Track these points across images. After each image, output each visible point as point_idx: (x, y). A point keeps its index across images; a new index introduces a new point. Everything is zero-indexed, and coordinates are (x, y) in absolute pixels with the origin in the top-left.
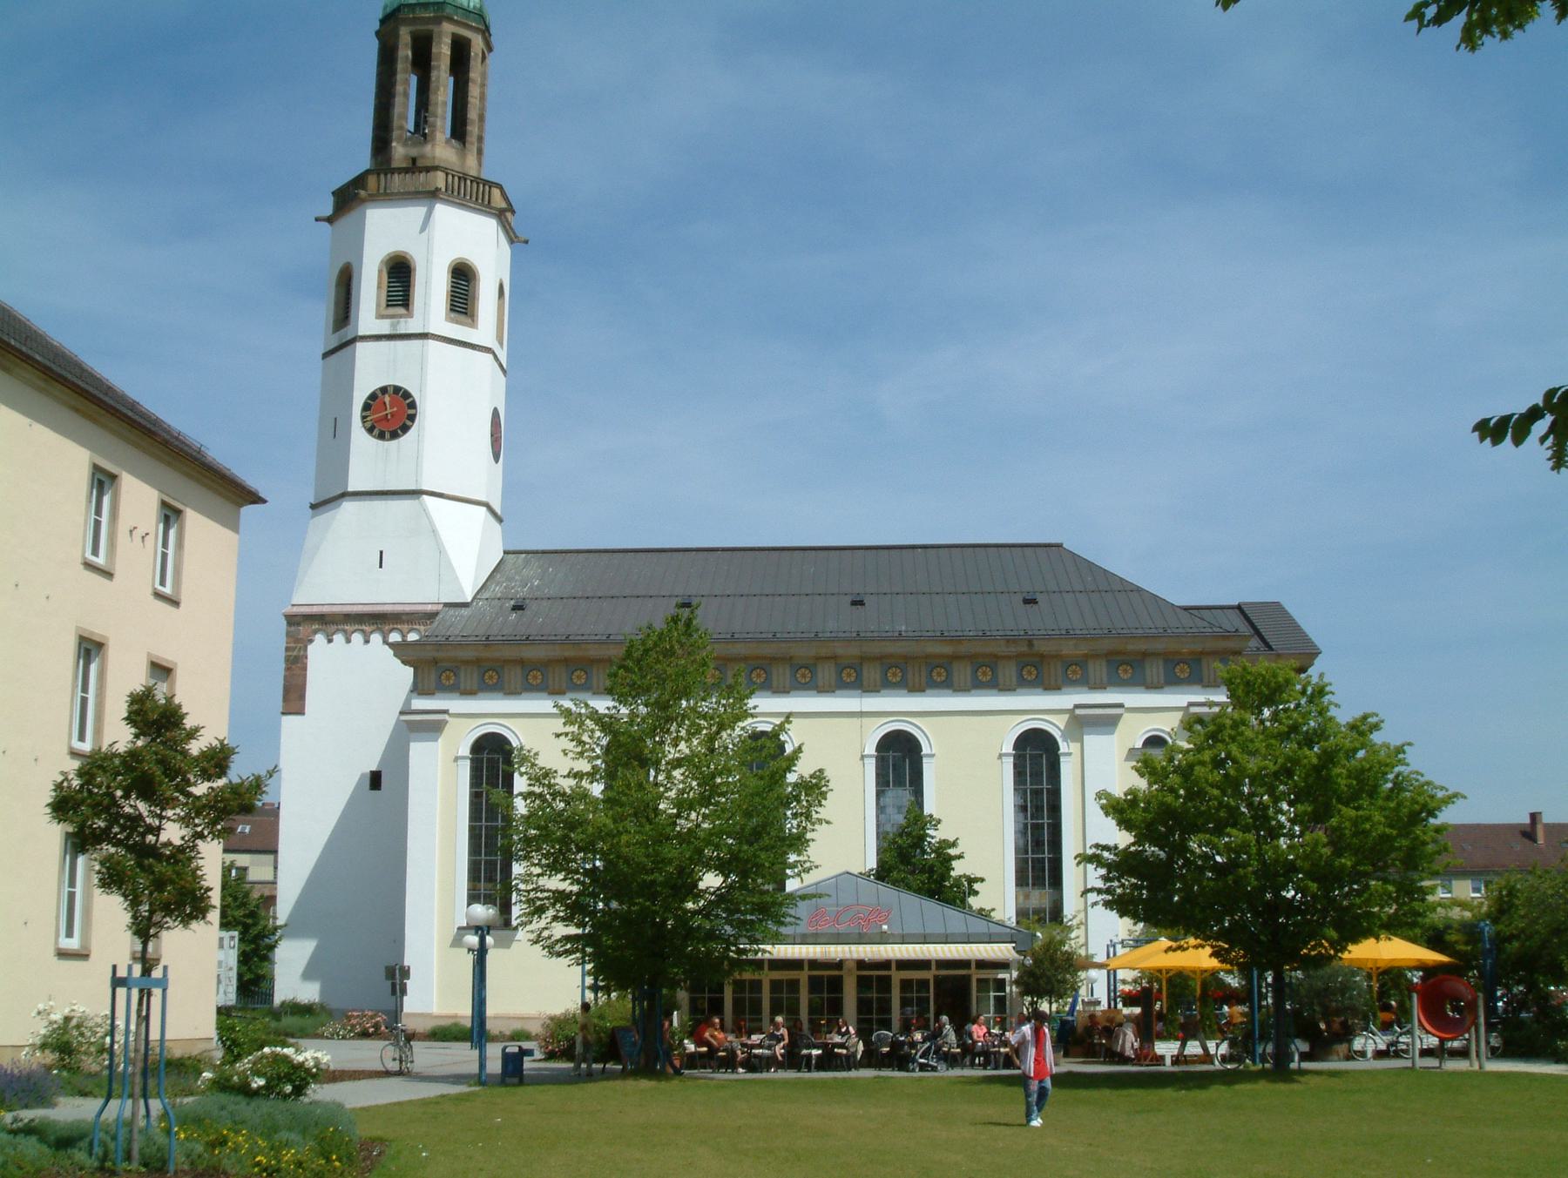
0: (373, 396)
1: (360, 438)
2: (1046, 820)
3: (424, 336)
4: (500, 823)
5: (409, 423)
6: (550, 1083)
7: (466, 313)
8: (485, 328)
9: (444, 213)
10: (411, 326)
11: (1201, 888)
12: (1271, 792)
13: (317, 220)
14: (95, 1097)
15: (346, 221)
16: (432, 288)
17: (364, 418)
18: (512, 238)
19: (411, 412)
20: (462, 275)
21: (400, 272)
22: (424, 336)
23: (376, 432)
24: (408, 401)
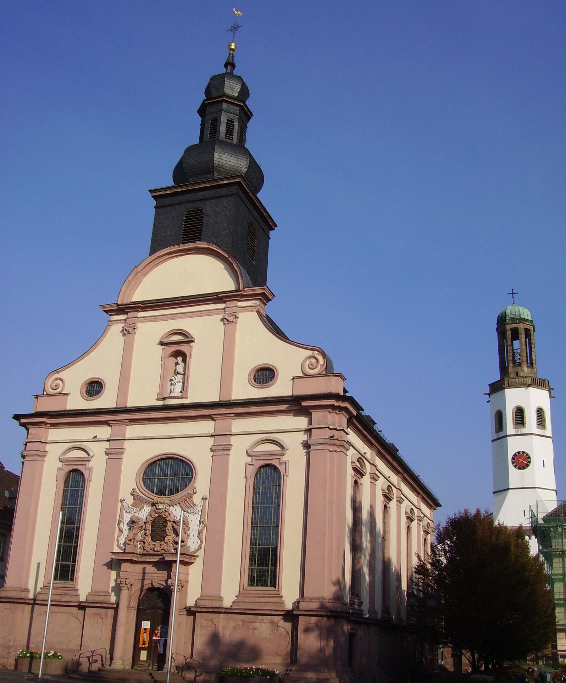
0: (515, 455)
1: (512, 469)
2: (270, 568)
3: (532, 434)
4: (78, 506)
5: (529, 464)
6: (29, 668)
7: (542, 425)
8: (548, 431)
9: (532, 390)
10: (524, 431)
11: (253, 671)
12: (434, 585)
13: (484, 394)
14: (287, 665)
15: (495, 396)
16: (531, 418)
17: (513, 463)
18: (551, 397)
19: (529, 460)
20: (540, 412)
21: (520, 413)
22: (532, 434)
23: (517, 467)
24: (528, 456)
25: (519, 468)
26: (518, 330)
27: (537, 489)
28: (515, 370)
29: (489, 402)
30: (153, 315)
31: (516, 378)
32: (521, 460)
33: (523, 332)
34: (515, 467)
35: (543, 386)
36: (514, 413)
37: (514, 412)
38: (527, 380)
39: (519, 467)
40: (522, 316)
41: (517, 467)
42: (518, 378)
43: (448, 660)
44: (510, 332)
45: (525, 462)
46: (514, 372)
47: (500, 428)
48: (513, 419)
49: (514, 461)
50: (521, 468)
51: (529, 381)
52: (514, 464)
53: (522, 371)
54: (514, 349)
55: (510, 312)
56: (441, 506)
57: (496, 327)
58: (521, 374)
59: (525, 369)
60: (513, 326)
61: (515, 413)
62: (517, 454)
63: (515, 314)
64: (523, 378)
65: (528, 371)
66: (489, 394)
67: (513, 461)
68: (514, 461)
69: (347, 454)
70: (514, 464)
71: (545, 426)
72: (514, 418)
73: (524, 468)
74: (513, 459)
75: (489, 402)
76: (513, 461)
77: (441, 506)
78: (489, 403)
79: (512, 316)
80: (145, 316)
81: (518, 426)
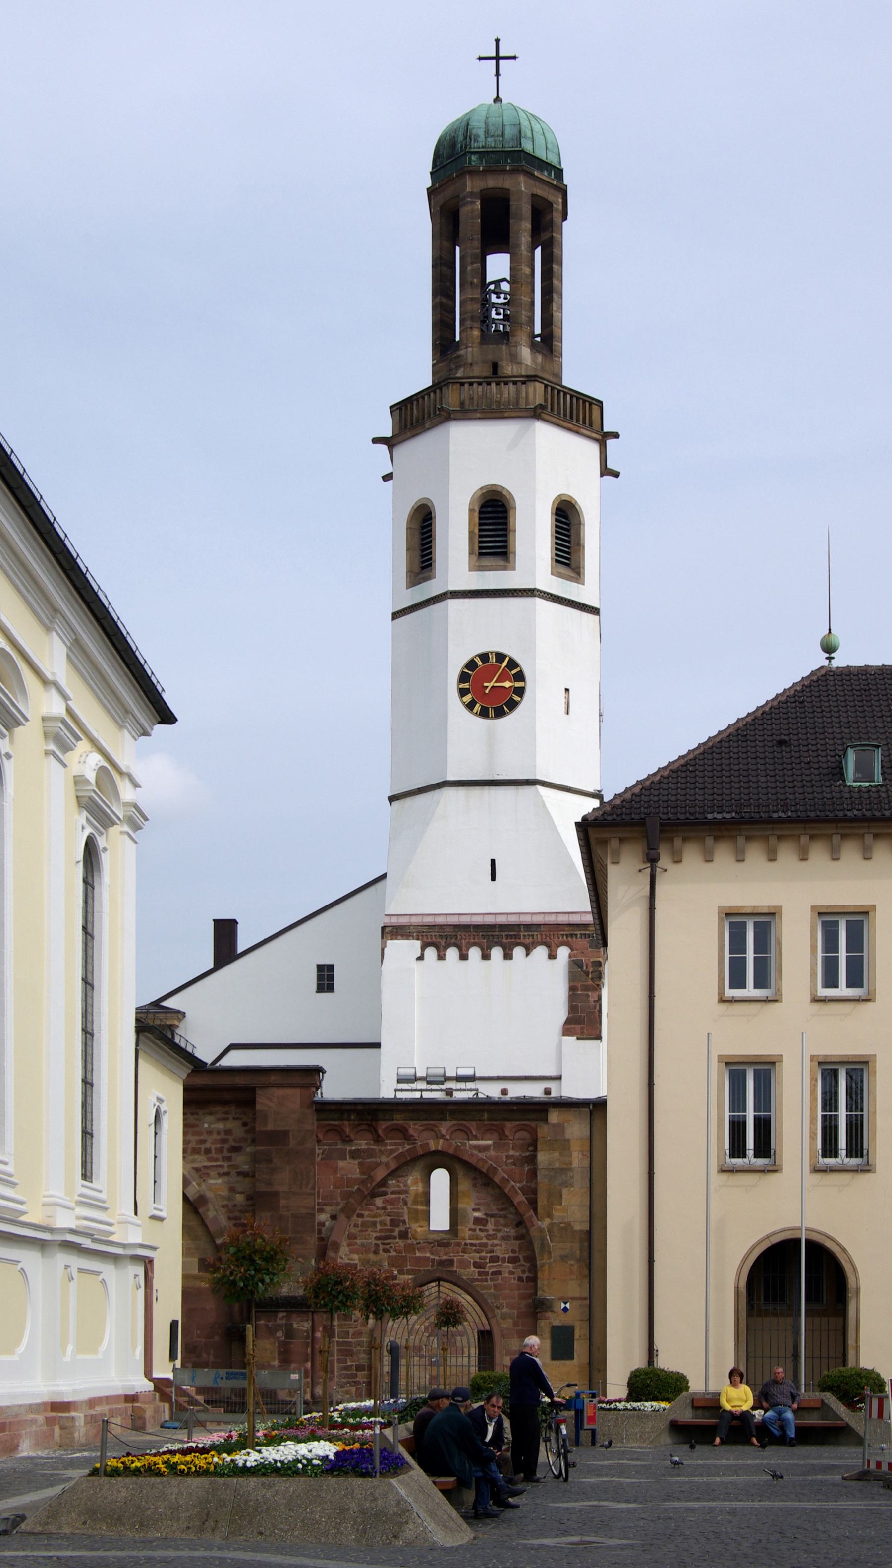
17: (463, 693)
23: (477, 708)
25: (484, 714)
26: (508, 200)
27: (540, 789)
28: (490, 357)
29: (387, 477)
30: (95, 734)
31: (489, 384)
32: (490, 685)
33: (526, 209)
34: (470, 706)
35: (584, 423)
36: (476, 515)
37: (477, 509)
38: (531, 390)
39: (482, 707)
40: (527, 146)
41: (477, 708)
42: (497, 384)
43: (204, 1355)
44: (478, 203)
45: (507, 684)
46: (484, 362)
47: (423, 568)
48: (471, 533)
49: (466, 686)
50: (491, 712)
51: (536, 393)
52: (468, 698)
53: (515, 358)
54: (488, 280)
55: (482, 125)
56: (140, 787)
57: (429, 184)
58: (508, 369)
59: (526, 353)
60: (492, 182)
61: (480, 513)
62: (480, 663)
63: (503, 135)
64: (515, 383)
65: (534, 360)
66: (390, 443)
67: (462, 686)
68: (466, 686)
69: (28, 716)
70: (468, 698)
71: (579, 567)
72: (477, 531)
73: (500, 713)
74: (463, 678)
75: (387, 477)
76: (462, 686)
77: (140, 787)
78: (391, 482)
79: (490, 141)
80: (104, 744)
81: (488, 561)
